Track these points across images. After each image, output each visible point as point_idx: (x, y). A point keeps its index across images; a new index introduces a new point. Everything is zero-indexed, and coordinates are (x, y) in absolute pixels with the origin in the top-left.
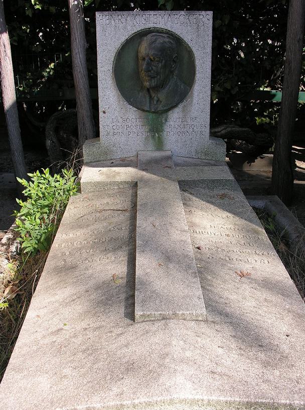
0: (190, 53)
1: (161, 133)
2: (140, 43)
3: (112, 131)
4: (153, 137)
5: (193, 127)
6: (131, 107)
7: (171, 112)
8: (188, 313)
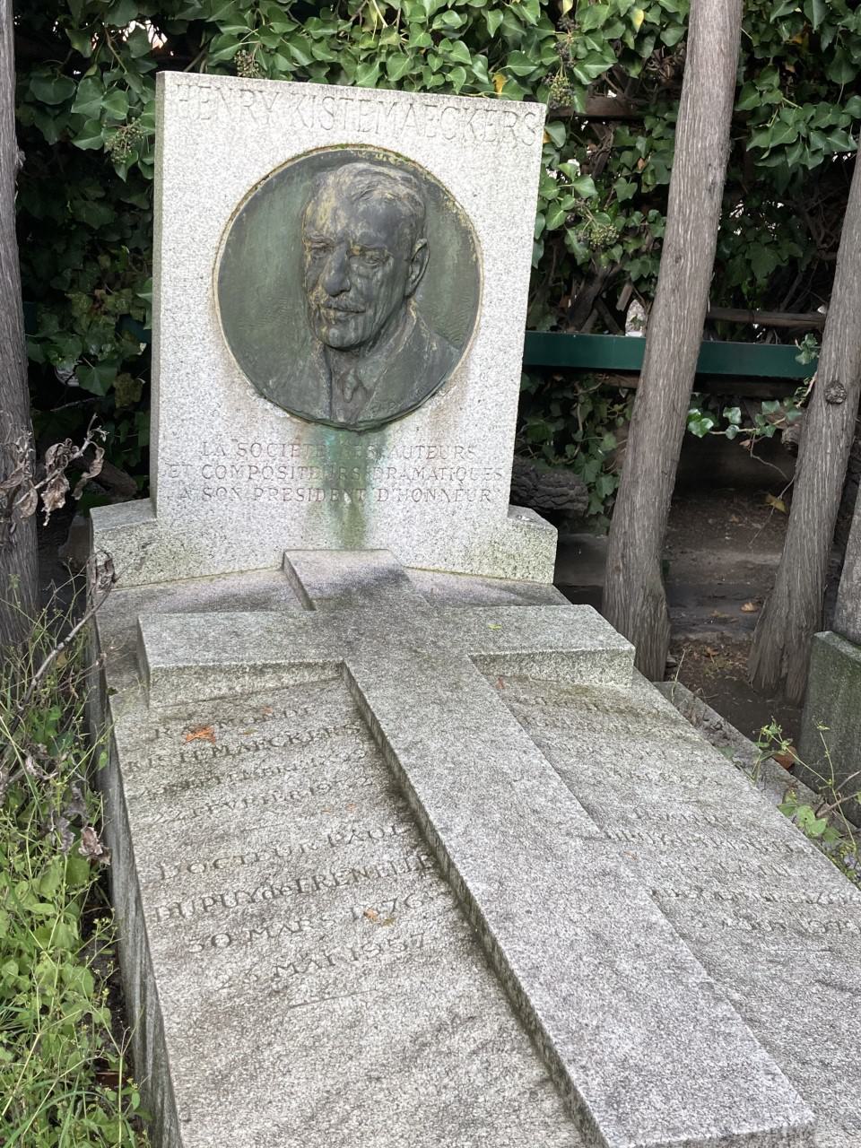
0: (467, 238)
1: (361, 495)
2: (314, 192)
3: (199, 483)
4: (336, 506)
5: (460, 473)
6: (269, 405)
7: (396, 426)
8: (767, 1128)
